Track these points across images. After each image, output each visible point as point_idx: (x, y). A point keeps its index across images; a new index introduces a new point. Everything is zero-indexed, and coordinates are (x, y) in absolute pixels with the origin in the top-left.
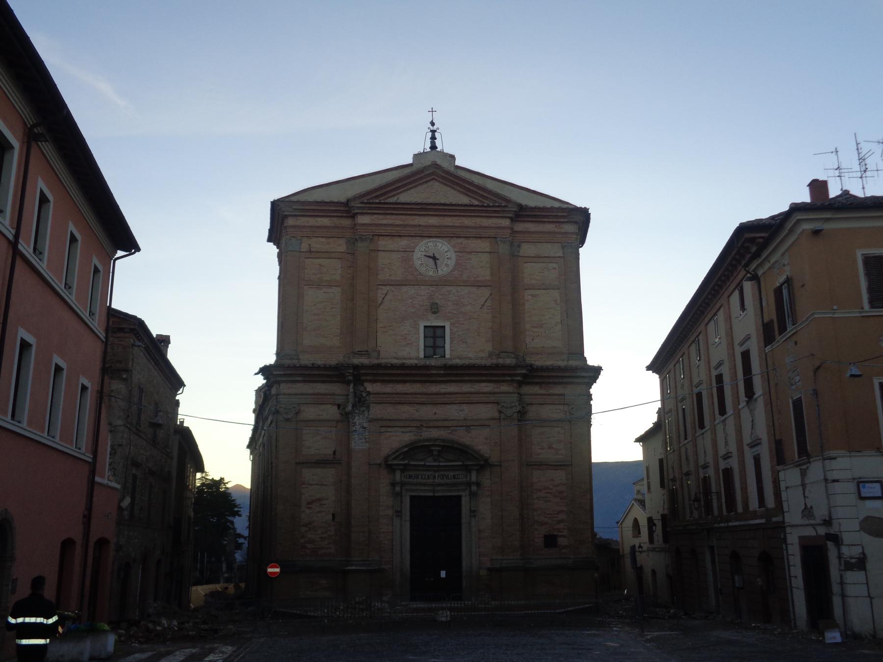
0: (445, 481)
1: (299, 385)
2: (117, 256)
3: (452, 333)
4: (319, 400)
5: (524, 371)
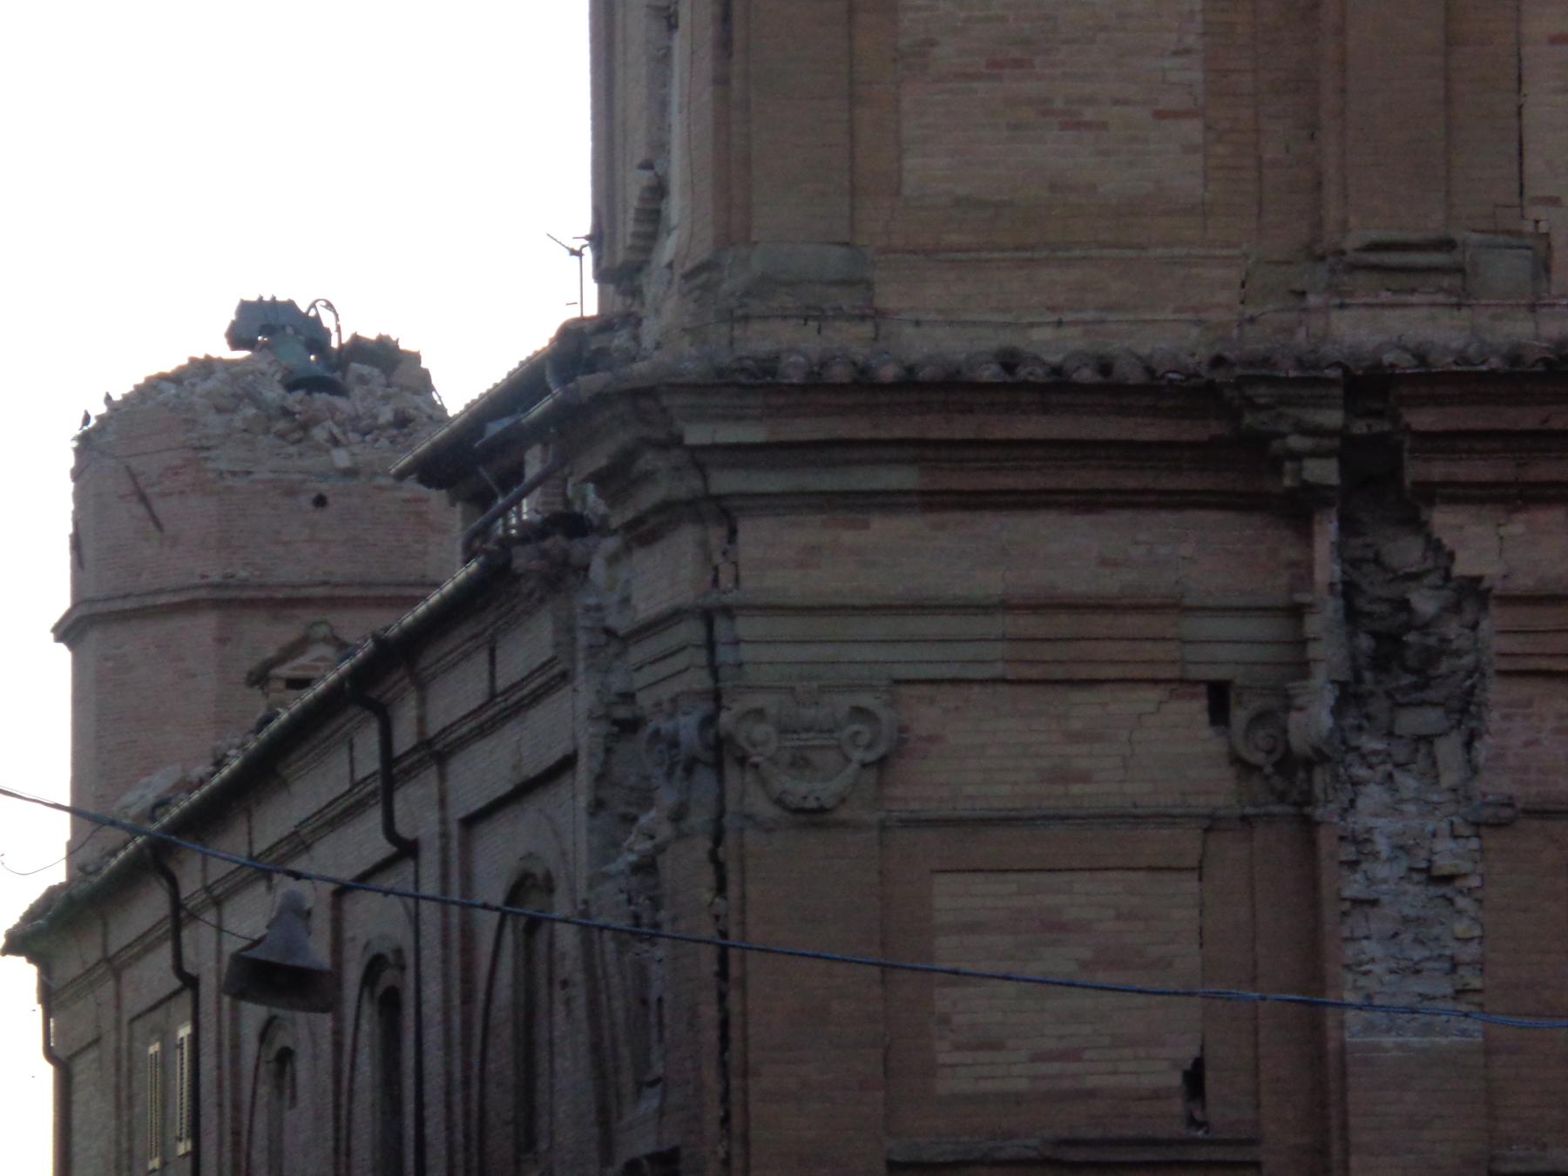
1: (885, 530)
4: (1053, 651)
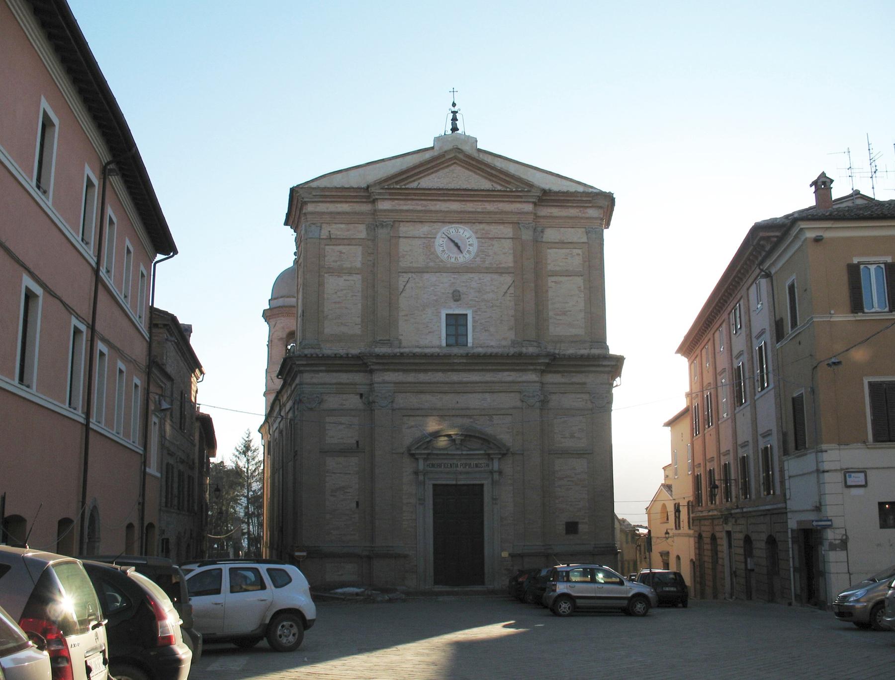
0: (467, 469)
1: (321, 374)
2: (157, 259)
3: (474, 321)
4: (341, 389)
5: (547, 361)
